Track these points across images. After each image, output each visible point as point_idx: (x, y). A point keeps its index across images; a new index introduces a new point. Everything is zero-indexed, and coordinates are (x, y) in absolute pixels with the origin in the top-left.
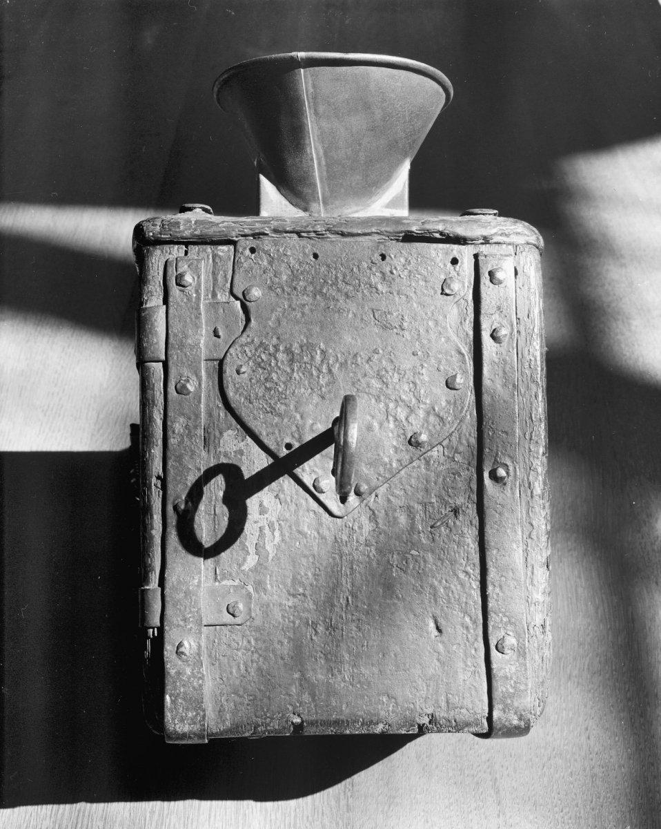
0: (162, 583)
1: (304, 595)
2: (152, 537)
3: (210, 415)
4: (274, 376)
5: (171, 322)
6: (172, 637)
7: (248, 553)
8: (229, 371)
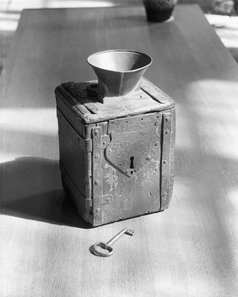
0: (92, 198)
1: (123, 194)
2: (89, 189)
3: (102, 161)
4: (117, 151)
5: (94, 143)
6: (95, 209)
7: (111, 188)
8: (107, 151)
